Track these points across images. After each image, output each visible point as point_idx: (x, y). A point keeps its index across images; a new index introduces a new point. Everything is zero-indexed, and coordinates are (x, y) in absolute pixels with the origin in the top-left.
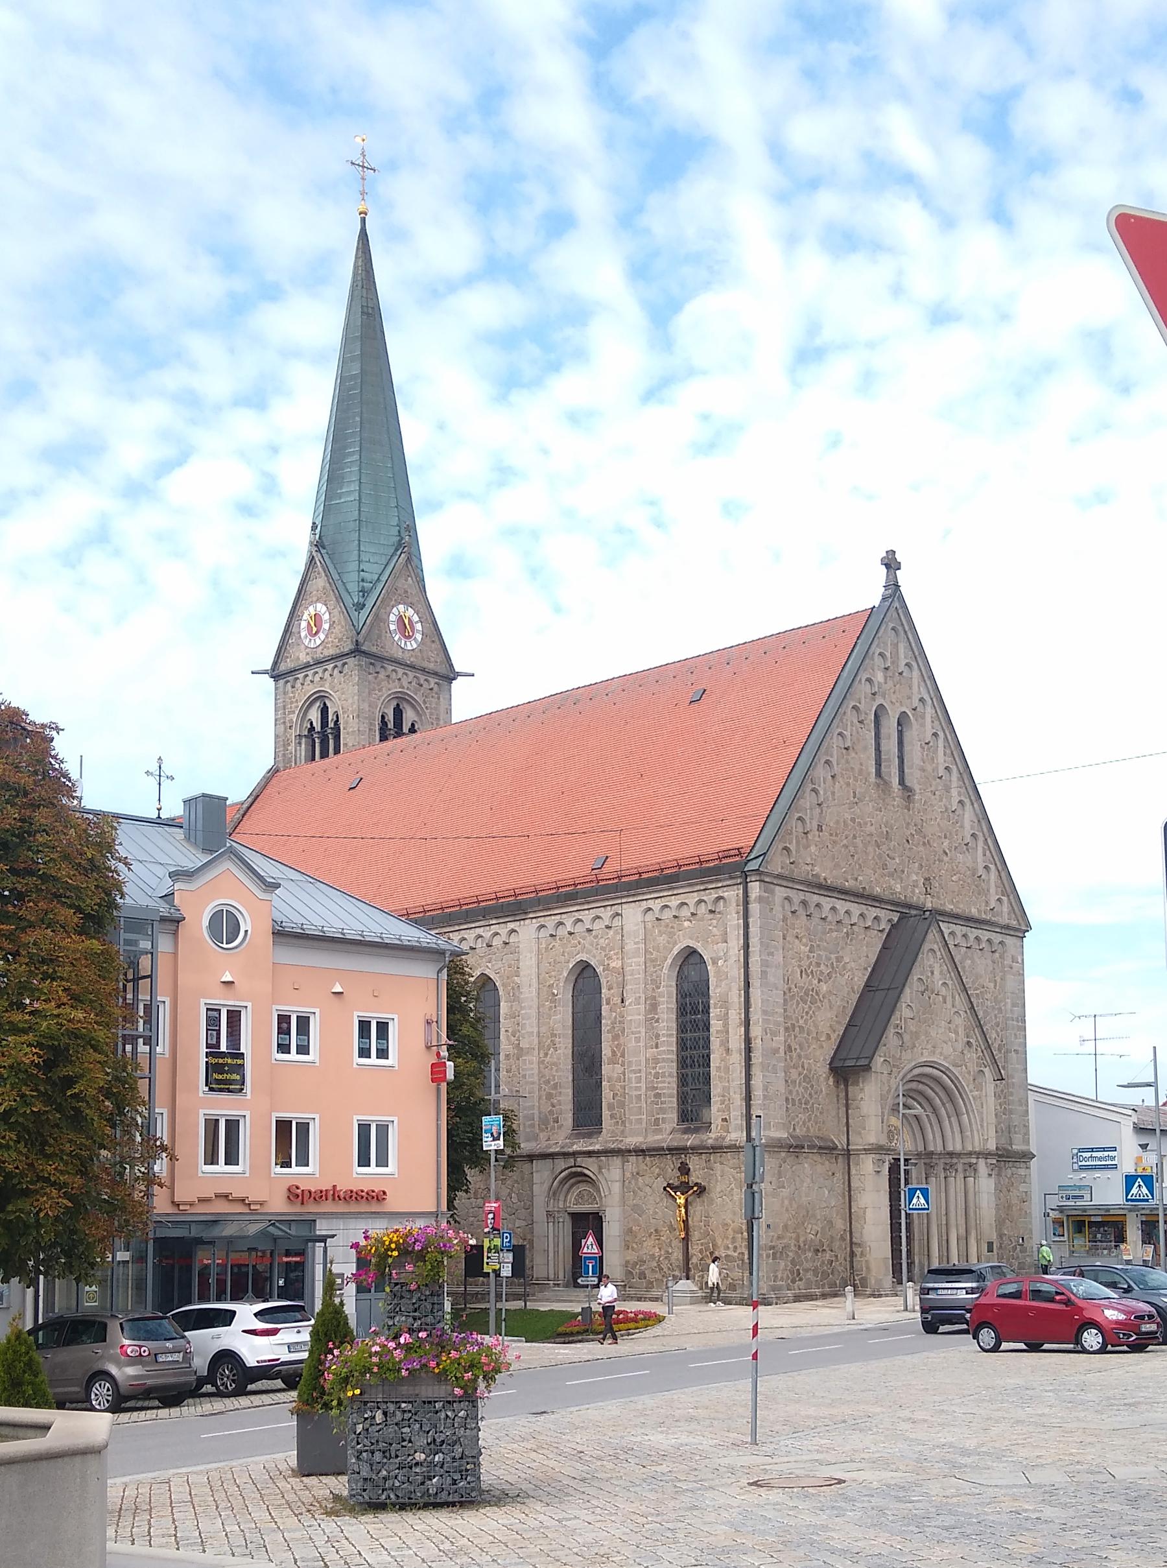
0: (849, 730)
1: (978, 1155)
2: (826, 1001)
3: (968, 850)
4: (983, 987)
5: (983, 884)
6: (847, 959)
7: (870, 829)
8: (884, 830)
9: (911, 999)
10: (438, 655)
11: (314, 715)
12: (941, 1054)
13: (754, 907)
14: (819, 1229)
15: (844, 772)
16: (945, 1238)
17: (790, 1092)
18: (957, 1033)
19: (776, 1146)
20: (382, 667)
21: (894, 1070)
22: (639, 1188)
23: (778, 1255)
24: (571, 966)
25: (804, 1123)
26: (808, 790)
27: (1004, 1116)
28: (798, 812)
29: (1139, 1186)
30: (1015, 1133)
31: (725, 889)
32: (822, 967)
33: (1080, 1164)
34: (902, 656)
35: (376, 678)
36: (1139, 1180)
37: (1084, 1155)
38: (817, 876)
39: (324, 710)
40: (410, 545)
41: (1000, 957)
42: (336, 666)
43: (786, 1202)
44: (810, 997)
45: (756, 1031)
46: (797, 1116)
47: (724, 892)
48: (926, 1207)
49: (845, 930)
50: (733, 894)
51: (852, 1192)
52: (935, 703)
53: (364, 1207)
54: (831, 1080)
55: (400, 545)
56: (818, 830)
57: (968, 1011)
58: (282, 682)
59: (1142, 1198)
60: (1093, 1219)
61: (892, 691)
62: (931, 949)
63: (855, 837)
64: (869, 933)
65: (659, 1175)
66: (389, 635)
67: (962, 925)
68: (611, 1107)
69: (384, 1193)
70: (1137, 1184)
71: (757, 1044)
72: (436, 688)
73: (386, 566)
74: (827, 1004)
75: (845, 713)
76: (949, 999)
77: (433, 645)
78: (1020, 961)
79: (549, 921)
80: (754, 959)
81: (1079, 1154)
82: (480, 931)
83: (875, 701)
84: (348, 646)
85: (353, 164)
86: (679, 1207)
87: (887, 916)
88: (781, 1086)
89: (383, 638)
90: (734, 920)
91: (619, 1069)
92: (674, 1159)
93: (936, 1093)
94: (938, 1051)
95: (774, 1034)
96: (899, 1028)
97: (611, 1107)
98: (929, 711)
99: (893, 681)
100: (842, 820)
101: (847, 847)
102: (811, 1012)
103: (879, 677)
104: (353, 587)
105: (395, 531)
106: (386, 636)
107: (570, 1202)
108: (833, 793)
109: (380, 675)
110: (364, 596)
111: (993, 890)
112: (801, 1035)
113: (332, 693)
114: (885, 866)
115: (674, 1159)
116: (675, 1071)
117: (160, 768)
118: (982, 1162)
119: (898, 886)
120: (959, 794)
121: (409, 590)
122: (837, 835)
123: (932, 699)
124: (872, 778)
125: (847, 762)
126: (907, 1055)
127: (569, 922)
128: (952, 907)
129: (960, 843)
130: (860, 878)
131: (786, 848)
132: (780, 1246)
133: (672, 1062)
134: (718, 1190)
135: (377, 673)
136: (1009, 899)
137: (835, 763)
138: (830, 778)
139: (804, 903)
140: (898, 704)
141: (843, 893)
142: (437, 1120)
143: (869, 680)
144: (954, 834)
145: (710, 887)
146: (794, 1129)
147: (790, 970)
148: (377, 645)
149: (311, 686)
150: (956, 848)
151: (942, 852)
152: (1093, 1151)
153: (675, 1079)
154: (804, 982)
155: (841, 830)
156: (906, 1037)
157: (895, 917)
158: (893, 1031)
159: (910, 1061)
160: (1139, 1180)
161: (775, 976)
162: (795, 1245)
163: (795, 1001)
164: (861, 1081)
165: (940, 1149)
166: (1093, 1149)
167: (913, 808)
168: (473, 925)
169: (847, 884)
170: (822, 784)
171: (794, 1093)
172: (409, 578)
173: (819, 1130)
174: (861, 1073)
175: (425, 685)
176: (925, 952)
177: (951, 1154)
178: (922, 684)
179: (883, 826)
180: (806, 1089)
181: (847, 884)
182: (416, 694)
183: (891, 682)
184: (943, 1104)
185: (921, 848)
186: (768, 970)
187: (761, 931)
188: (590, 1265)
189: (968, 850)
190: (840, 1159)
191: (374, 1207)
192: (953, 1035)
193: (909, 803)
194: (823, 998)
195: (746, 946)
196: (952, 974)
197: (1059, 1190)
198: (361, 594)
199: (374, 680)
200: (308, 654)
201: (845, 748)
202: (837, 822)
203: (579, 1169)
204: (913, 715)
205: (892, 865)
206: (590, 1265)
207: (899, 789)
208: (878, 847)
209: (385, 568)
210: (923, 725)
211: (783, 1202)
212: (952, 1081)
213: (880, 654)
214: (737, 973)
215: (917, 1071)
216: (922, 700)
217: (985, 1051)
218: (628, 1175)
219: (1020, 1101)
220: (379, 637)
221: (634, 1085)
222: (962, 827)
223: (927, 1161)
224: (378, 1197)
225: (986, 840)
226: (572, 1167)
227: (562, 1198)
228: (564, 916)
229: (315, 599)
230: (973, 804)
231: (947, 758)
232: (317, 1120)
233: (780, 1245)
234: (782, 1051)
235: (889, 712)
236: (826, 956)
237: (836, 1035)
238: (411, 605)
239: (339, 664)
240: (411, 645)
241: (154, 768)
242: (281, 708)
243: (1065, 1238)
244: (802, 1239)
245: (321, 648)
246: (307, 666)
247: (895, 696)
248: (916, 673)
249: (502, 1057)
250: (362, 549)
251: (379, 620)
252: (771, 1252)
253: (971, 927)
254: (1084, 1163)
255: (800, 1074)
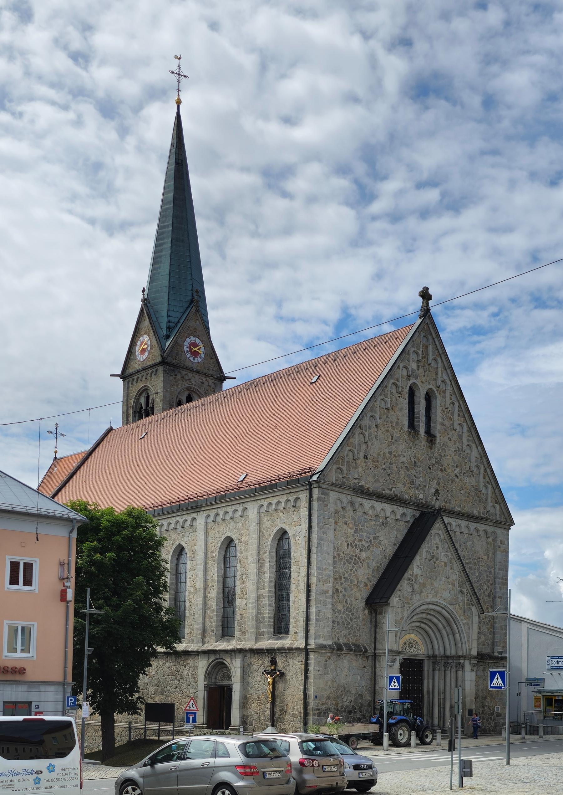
0: (389, 397)
1: (465, 657)
2: (365, 563)
3: (473, 475)
4: (480, 559)
5: (482, 496)
6: (381, 538)
7: (402, 459)
8: (413, 460)
9: (420, 563)
10: (214, 366)
11: (143, 401)
12: (441, 597)
13: (315, 504)
14: (353, 699)
15: (385, 423)
16: (442, 706)
17: (336, 617)
18: (453, 585)
19: (321, 648)
20: (179, 372)
21: (406, 605)
22: (251, 672)
23: (322, 714)
24: (223, 539)
25: (346, 636)
26: (357, 433)
27: (490, 636)
28: (349, 446)
29: (498, 678)
30: (497, 646)
31: (300, 493)
32: (364, 543)
33: (551, 665)
34: (430, 353)
35: (175, 378)
36: (498, 674)
37: (554, 660)
38: (362, 486)
39: (148, 398)
40: (198, 302)
41: (493, 540)
42: (153, 372)
43: (329, 683)
44: (354, 560)
45: (313, 580)
46: (341, 632)
47: (300, 494)
48: (399, 688)
49: (381, 520)
50: (304, 496)
51: (376, 678)
52: (453, 384)
53: (10, 677)
54: (366, 612)
55: (192, 301)
56: (364, 458)
57: (462, 572)
58: (126, 381)
59: (498, 686)
60: (557, 698)
61: (423, 374)
62: (437, 533)
63: (391, 464)
64: (398, 523)
65: (261, 665)
66: (183, 353)
67: (465, 520)
68: (240, 625)
69: (24, 669)
70: (496, 677)
71: (313, 588)
72: (213, 386)
73: (184, 313)
74: (366, 565)
75: (386, 387)
76: (449, 564)
77: (211, 361)
78: (506, 543)
79: (212, 512)
80: (314, 536)
81: (551, 660)
82: (178, 518)
83: (410, 380)
84: (159, 359)
85: (172, 72)
86: (269, 684)
87: (410, 514)
88: (329, 614)
89: (180, 355)
90: (304, 512)
91: (244, 601)
92: (269, 655)
93: (439, 620)
94: (439, 595)
95: (325, 582)
96: (411, 580)
97: (240, 625)
98: (449, 389)
99: (424, 369)
100: (382, 453)
101: (385, 470)
102: (354, 570)
103: (414, 366)
104: (164, 325)
105: (190, 293)
106: (182, 354)
107: (218, 680)
108: (376, 436)
109: (177, 377)
110: (170, 330)
111: (489, 500)
112: (346, 583)
113: (151, 387)
114: (412, 482)
115: (269, 655)
116: (273, 603)
117: (57, 429)
118: (467, 663)
119: (422, 495)
120: (468, 440)
121: (197, 328)
122: (378, 461)
123: (451, 381)
124: (406, 428)
125: (388, 417)
126: (416, 597)
127: (221, 513)
128: (460, 509)
129: (467, 471)
130: (393, 489)
131: (339, 468)
132: (324, 709)
133: (272, 598)
134: (291, 674)
135: (176, 375)
136: (500, 506)
137: (378, 418)
138: (375, 426)
139: (352, 504)
140: (426, 384)
141: (380, 497)
142: (66, 625)
143: (405, 367)
144: (463, 465)
145: (292, 492)
146: (338, 639)
147: (339, 544)
148: (176, 359)
149: (141, 383)
150: (464, 473)
151: (454, 476)
152: (558, 658)
153: (273, 608)
154: (349, 551)
155: (381, 459)
156: (416, 587)
157: (417, 514)
158: (406, 582)
159: (418, 601)
160: (498, 674)
161: (328, 547)
162: (335, 709)
163: (342, 562)
164: (383, 612)
165: (453, 653)
166: (559, 657)
167: (435, 448)
168: (174, 515)
169: (384, 492)
170: (368, 430)
171: (339, 618)
172: (198, 321)
173: (356, 640)
174: (384, 607)
175: (206, 383)
176: (433, 534)
177: (447, 657)
178: (444, 371)
179: (412, 458)
180: (348, 615)
181: (384, 492)
182: (200, 388)
183: (422, 369)
184: (444, 627)
185: (440, 473)
186: (322, 542)
187: (318, 518)
188: (191, 717)
189: (473, 475)
190: (370, 659)
191: (18, 677)
192: (451, 586)
193: (432, 444)
194: (363, 561)
195: (310, 528)
196: (451, 549)
197: (526, 680)
198: (168, 329)
199: (173, 379)
200: (139, 365)
201: (386, 409)
202: (379, 454)
203: (221, 660)
204: (438, 391)
205: (417, 482)
206: (191, 717)
207: (425, 436)
208: (408, 470)
209: (183, 314)
210: (444, 397)
211: (327, 682)
212: (449, 614)
213: (415, 352)
214: (304, 543)
215: (423, 607)
216: (444, 381)
217: (472, 596)
218: (246, 664)
219: (501, 627)
220: (177, 354)
221: (250, 611)
222: (470, 461)
223: (434, 661)
224: (22, 671)
225: (486, 469)
226: (217, 659)
227: (214, 677)
228: (219, 510)
229: (143, 333)
230: (477, 447)
231: (460, 418)
232: (36, 626)
233: (323, 708)
234: (330, 593)
235: (421, 389)
236: (366, 536)
237: (371, 584)
238: (198, 337)
239: (154, 370)
240: (198, 360)
241: (53, 429)
242: (127, 395)
243: (541, 709)
244: (340, 705)
245: (146, 361)
246: (138, 371)
247: (425, 378)
248: (440, 365)
249: (187, 593)
250: (170, 303)
251: (176, 345)
252: (317, 712)
253: (472, 522)
254: (553, 665)
255: (344, 606)
